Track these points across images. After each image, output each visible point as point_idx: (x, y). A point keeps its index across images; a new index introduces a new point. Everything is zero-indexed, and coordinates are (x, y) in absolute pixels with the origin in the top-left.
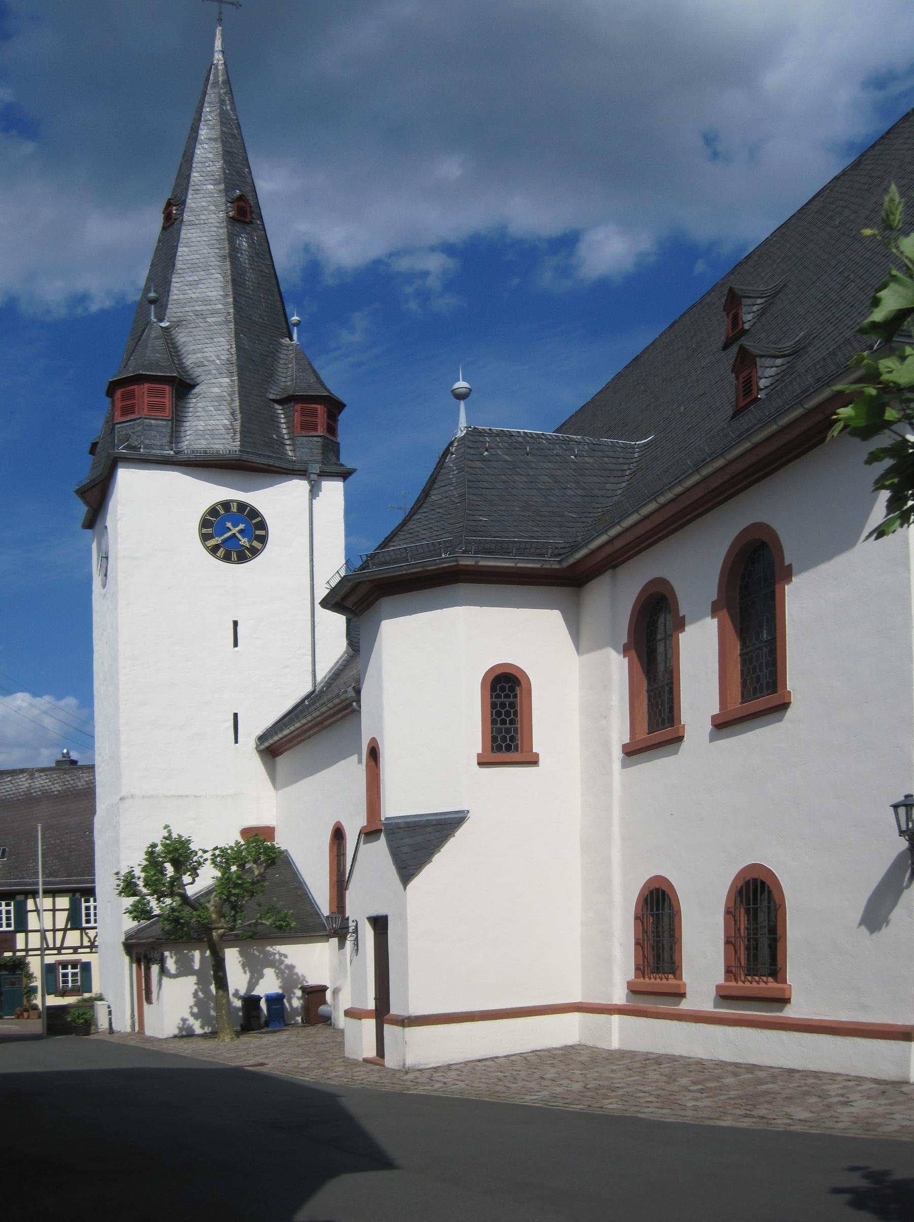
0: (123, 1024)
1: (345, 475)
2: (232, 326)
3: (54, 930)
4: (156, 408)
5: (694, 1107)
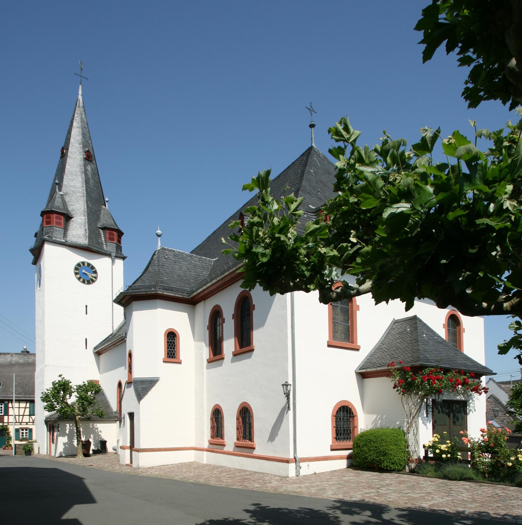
0: (44, 452)
1: (124, 258)
2: (85, 198)
3: (19, 416)
4: (59, 224)
5: (226, 481)
